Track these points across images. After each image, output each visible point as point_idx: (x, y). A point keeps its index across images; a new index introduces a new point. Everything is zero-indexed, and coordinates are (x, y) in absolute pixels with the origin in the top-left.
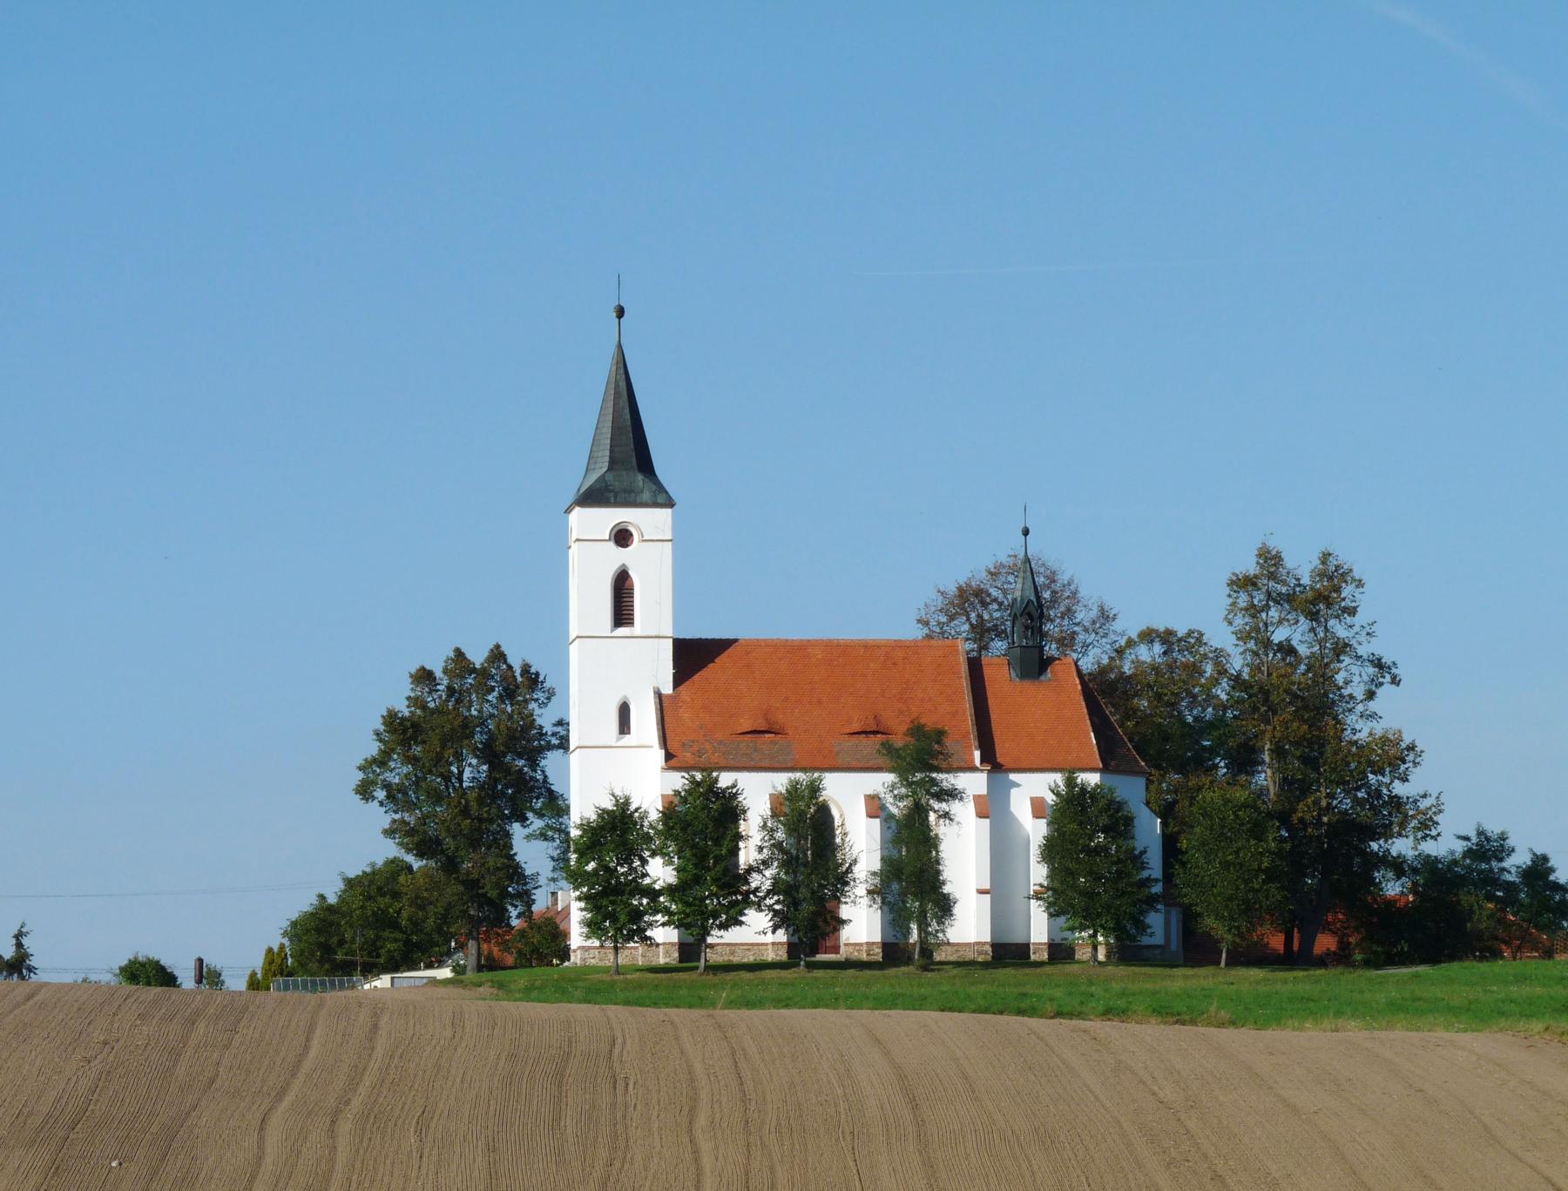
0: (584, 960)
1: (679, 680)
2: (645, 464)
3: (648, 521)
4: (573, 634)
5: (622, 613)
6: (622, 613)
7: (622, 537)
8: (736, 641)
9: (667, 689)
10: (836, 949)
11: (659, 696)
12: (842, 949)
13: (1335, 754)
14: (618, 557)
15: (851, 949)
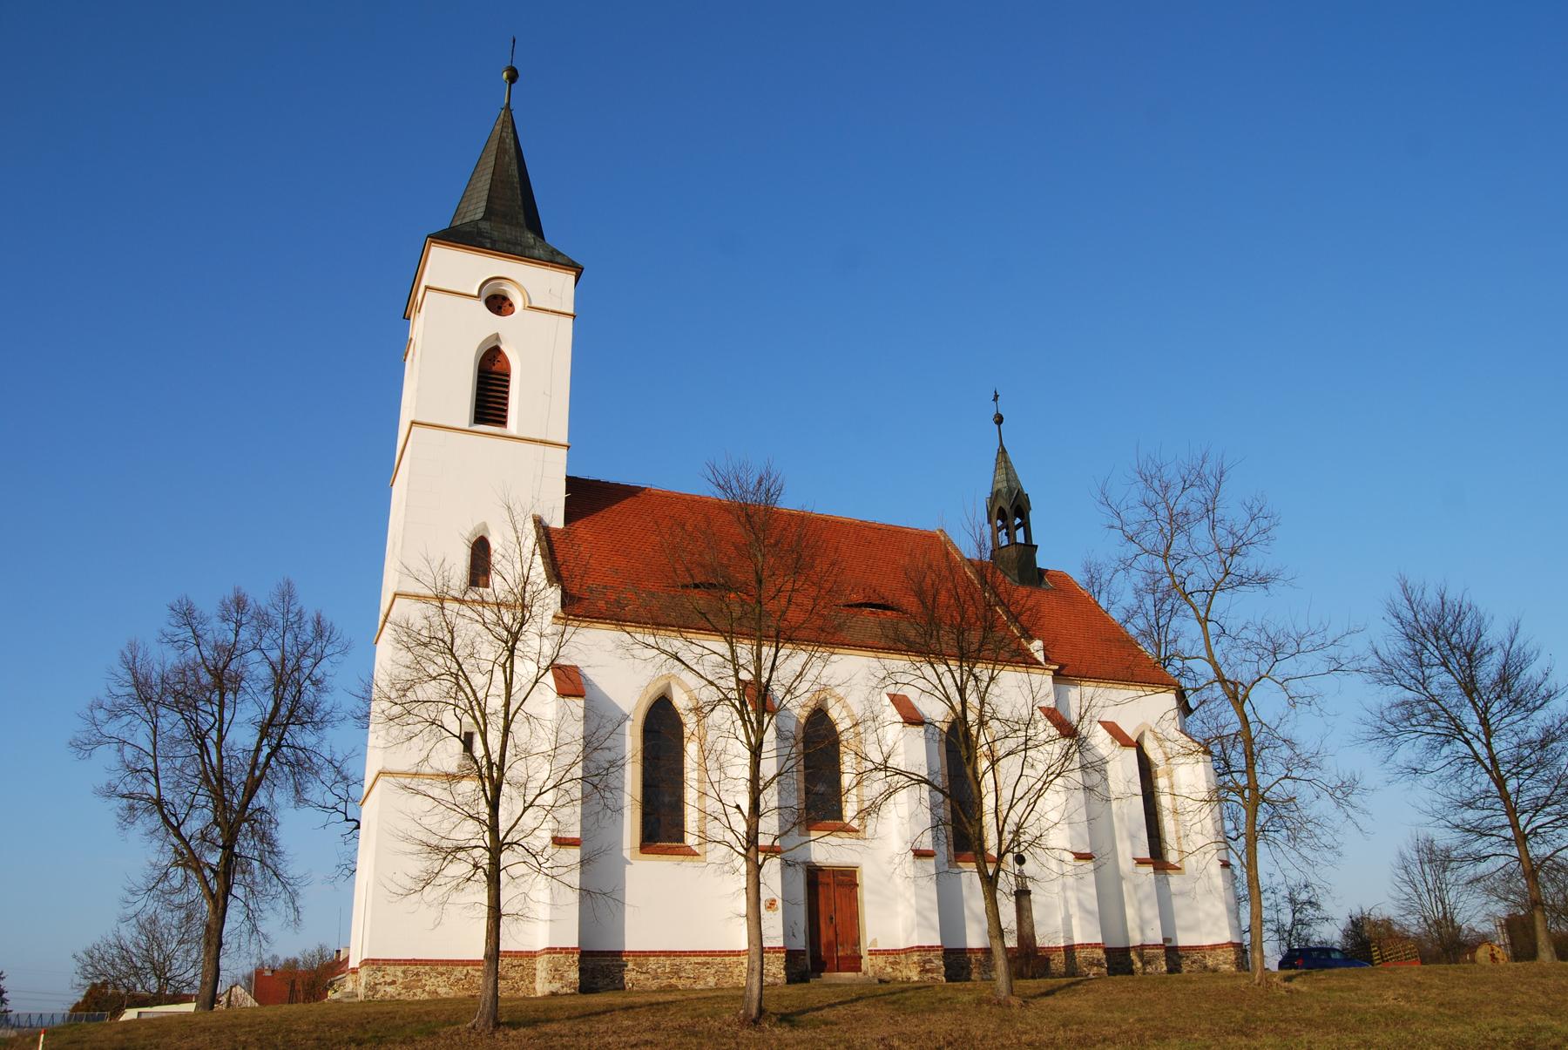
0: (372, 988)
1: (570, 515)
2: (533, 223)
3: (542, 287)
4: (406, 416)
5: (490, 401)
6: (490, 401)
7: (498, 303)
8: (630, 492)
9: (557, 521)
10: (854, 963)
11: (544, 533)
12: (866, 962)
13: (113, 966)
14: (487, 324)
15: (880, 961)
